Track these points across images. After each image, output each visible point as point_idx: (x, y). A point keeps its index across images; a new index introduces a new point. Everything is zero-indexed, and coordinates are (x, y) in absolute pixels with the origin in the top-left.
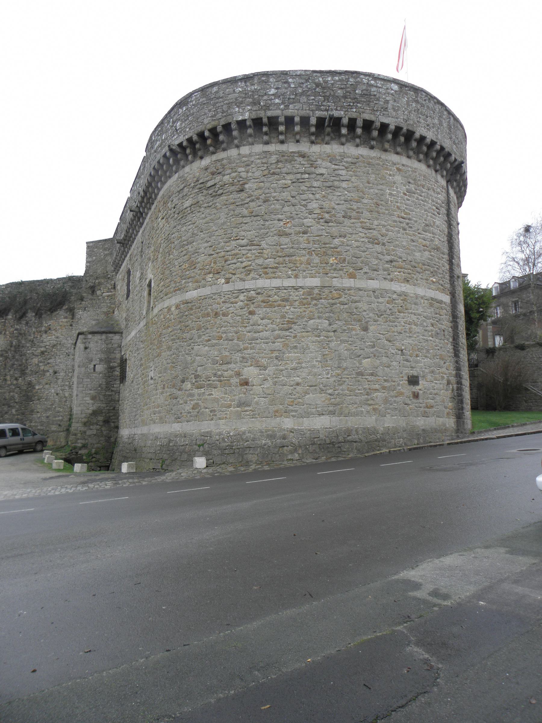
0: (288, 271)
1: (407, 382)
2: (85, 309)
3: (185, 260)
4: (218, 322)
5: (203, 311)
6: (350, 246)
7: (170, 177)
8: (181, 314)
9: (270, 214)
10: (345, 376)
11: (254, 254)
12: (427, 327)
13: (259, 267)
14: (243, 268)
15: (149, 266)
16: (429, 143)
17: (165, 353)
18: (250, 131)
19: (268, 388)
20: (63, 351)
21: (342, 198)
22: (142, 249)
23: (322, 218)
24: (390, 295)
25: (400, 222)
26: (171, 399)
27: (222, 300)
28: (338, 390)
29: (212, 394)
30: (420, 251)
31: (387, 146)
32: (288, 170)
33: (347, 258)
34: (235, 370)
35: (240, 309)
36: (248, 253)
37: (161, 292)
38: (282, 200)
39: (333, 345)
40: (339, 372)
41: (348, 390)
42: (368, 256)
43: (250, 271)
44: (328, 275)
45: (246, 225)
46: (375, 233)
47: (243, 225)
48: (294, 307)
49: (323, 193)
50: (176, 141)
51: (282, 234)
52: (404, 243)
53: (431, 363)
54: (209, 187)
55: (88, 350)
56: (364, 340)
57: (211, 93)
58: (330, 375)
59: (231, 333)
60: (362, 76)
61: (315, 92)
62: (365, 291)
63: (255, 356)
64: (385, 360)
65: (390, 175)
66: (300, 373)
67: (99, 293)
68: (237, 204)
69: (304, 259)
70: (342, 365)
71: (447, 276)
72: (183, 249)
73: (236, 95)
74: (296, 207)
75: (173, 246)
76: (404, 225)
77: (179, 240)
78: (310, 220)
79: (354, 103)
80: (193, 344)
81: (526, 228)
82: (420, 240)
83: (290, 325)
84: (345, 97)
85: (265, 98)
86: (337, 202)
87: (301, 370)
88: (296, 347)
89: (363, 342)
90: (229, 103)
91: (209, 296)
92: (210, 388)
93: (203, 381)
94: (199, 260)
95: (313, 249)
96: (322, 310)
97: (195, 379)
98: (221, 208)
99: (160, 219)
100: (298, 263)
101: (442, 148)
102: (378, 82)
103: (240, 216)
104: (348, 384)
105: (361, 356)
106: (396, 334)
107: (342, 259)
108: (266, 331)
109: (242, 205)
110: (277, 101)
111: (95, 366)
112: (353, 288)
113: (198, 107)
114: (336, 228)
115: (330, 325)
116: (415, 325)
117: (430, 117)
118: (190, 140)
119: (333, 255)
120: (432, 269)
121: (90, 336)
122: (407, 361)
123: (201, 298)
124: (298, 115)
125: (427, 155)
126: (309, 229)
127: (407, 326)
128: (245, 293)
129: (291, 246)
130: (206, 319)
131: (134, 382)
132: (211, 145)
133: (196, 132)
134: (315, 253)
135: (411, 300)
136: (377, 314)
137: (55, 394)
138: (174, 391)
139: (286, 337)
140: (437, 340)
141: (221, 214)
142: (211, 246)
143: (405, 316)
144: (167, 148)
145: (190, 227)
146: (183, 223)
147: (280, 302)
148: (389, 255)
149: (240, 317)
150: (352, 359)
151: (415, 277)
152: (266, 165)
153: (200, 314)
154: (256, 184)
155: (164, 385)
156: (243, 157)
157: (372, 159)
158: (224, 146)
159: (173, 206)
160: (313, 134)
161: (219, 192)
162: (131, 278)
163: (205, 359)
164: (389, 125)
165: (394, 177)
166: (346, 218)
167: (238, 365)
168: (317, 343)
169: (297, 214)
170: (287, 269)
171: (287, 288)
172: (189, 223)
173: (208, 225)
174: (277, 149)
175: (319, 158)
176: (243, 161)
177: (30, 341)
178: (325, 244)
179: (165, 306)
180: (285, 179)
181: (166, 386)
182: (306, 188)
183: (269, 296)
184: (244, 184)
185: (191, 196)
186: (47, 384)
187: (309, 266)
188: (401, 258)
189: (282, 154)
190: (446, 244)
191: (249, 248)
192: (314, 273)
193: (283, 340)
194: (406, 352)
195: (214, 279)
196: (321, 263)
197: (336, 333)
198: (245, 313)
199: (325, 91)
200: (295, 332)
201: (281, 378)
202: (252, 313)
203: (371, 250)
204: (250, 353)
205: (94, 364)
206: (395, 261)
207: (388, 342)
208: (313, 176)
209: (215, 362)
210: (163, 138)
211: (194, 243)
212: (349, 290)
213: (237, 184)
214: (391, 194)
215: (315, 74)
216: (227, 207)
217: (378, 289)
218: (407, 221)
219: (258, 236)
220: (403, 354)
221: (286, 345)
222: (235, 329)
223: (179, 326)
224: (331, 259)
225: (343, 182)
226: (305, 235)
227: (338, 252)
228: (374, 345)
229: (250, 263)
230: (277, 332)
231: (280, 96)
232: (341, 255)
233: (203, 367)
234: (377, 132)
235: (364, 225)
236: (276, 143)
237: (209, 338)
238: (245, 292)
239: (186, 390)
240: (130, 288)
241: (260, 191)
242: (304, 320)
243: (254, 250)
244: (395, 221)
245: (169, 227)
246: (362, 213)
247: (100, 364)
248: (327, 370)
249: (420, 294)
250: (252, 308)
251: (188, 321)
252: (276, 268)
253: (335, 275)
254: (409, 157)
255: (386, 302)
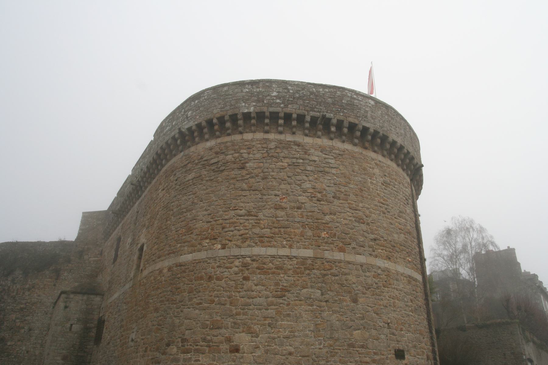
0: (283, 241)
1: (394, 356)
2: (70, 271)
3: (182, 226)
4: (211, 286)
5: (196, 275)
6: (340, 223)
7: (175, 155)
8: (173, 276)
9: (268, 190)
10: (337, 347)
11: (251, 223)
12: (407, 302)
13: (255, 236)
14: (239, 236)
15: (143, 232)
16: (399, 147)
17: (151, 315)
18: (253, 121)
19: (259, 357)
20: (42, 310)
21: (332, 182)
22: (137, 218)
23: (314, 197)
24: (375, 270)
25: (380, 207)
26: (152, 363)
27: (217, 265)
28: (330, 361)
29: (199, 360)
30: (397, 233)
31: (367, 144)
32: (285, 155)
33: (337, 234)
34: (226, 336)
35: (235, 274)
36: (245, 222)
37: (154, 255)
38: (279, 178)
39: (325, 315)
40: (331, 342)
41: (340, 362)
42: (356, 233)
43: (247, 239)
44: (320, 248)
45: (245, 198)
46: (360, 213)
47: (241, 197)
48: (289, 275)
49: (316, 176)
50: (186, 126)
51: (278, 207)
52: (385, 225)
53: (413, 337)
54: (212, 164)
55: (68, 309)
56: (355, 312)
57: (222, 91)
58: (322, 345)
59: (223, 297)
60: (346, 91)
61: (310, 98)
62: (354, 265)
63: (248, 322)
64: (374, 332)
65: (370, 168)
66: (292, 342)
67: (86, 257)
68: (238, 179)
69: (298, 231)
70: (334, 336)
71: (418, 258)
72: (181, 216)
73: (243, 94)
74: (291, 185)
75: (171, 212)
76: (384, 209)
77: (178, 208)
78: (304, 197)
79: (341, 109)
80: (183, 307)
81: (447, 231)
82: (396, 224)
83: (284, 293)
84: (334, 104)
85: (268, 98)
86: (327, 185)
87: (294, 339)
88: (288, 315)
89: (354, 313)
90: (237, 99)
91: (203, 260)
92: (197, 354)
93: (191, 345)
94: (197, 226)
95: (307, 223)
96: (315, 280)
97: (182, 343)
98: (222, 182)
99: (160, 191)
100: (293, 234)
101: (408, 153)
102: (359, 97)
103: (240, 189)
104: (340, 356)
105: (352, 328)
106: (382, 307)
107: (333, 234)
108: (260, 297)
109: (242, 180)
110: (278, 101)
111: (72, 325)
112: (343, 261)
113: (209, 101)
114: (327, 206)
115: (322, 294)
116: (398, 300)
117: (399, 127)
118: (199, 126)
119: (324, 230)
120: (407, 250)
121: (72, 296)
122: (393, 334)
123: (195, 261)
124: (296, 113)
125: (397, 156)
126: (303, 205)
127: (391, 300)
128: (240, 259)
129: (286, 219)
130: (199, 282)
131: (111, 344)
132: (217, 131)
133: (205, 119)
134: (308, 227)
135: (393, 276)
136: (365, 287)
137: (25, 352)
138: (157, 354)
139: (280, 304)
140: (416, 315)
141: (222, 187)
142: (210, 214)
143: (389, 291)
144: (177, 131)
145: (190, 197)
146: (184, 193)
147: (274, 270)
148: (373, 234)
149: (233, 282)
150: (343, 330)
151: (395, 256)
152: (266, 150)
153: (193, 277)
154: (256, 164)
155: (146, 348)
156: (246, 142)
157: (355, 153)
158: (229, 131)
159: (175, 179)
160: (307, 129)
161: (221, 169)
162: (121, 244)
163: (194, 323)
164: (369, 128)
165: (373, 169)
166: (336, 198)
167: (229, 331)
168: (310, 312)
169: (292, 192)
170: (282, 239)
171: (281, 257)
172: (190, 193)
173: (209, 196)
174: (276, 137)
175: (312, 148)
176: (245, 144)
177: (12, 297)
178: (317, 219)
179: (157, 268)
180: (282, 162)
181: (149, 349)
182: (300, 171)
183: (264, 264)
184: (246, 163)
185: (195, 171)
186: (19, 341)
187: (303, 238)
188: (383, 238)
189: (280, 142)
190: (415, 231)
191: (246, 217)
192: (307, 244)
193: (276, 307)
194: (392, 325)
195: (210, 244)
196: (314, 236)
197: (328, 303)
198: (239, 278)
199: (318, 98)
200: (288, 300)
201: (273, 346)
202: (246, 279)
203: (358, 228)
204: (242, 318)
205: (71, 323)
206: (378, 240)
207: (375, 315)
208: (307, 161)
209: (204, 326)
210: (174, 124)
211: (193, 211)
212: (339, 262)
213: (239, 162)
214: (371, 183)
215: (309, 86)
216: (228, 181)
217: (365, 264)
218: (386, 206)
219: (255, 208)
220: (389, 327)
221: (278, 313)
222: (228, 293)
223: (169, 288)
224: (323, 233)
225: (332, 168)
226: (299, 210)
227: (329, 227)
228: (363, 316)
229: (247, 231)
230: (270, 299)
231: (280, 98)
232: (332, 230)
233: (192, 331)
234: (360, 132)
235: (351, 206)
236: (275, 133)
237: (200, 301)
238: (240, 258)
239: (171, 355)
240: (119, 253)
241: (259, 170)
242: (297, 289)
243: (251, 220)
244: (376, 205)
245: (170, 196)
246: (349, 196)
247: (77, 324)
248: (319, 340)
249: (400, 271)
250: (246, 273)
251: (179, 283)
252: (272, 237)
253: (326, 248)
254: (384, 156)
255: (372, 276)
